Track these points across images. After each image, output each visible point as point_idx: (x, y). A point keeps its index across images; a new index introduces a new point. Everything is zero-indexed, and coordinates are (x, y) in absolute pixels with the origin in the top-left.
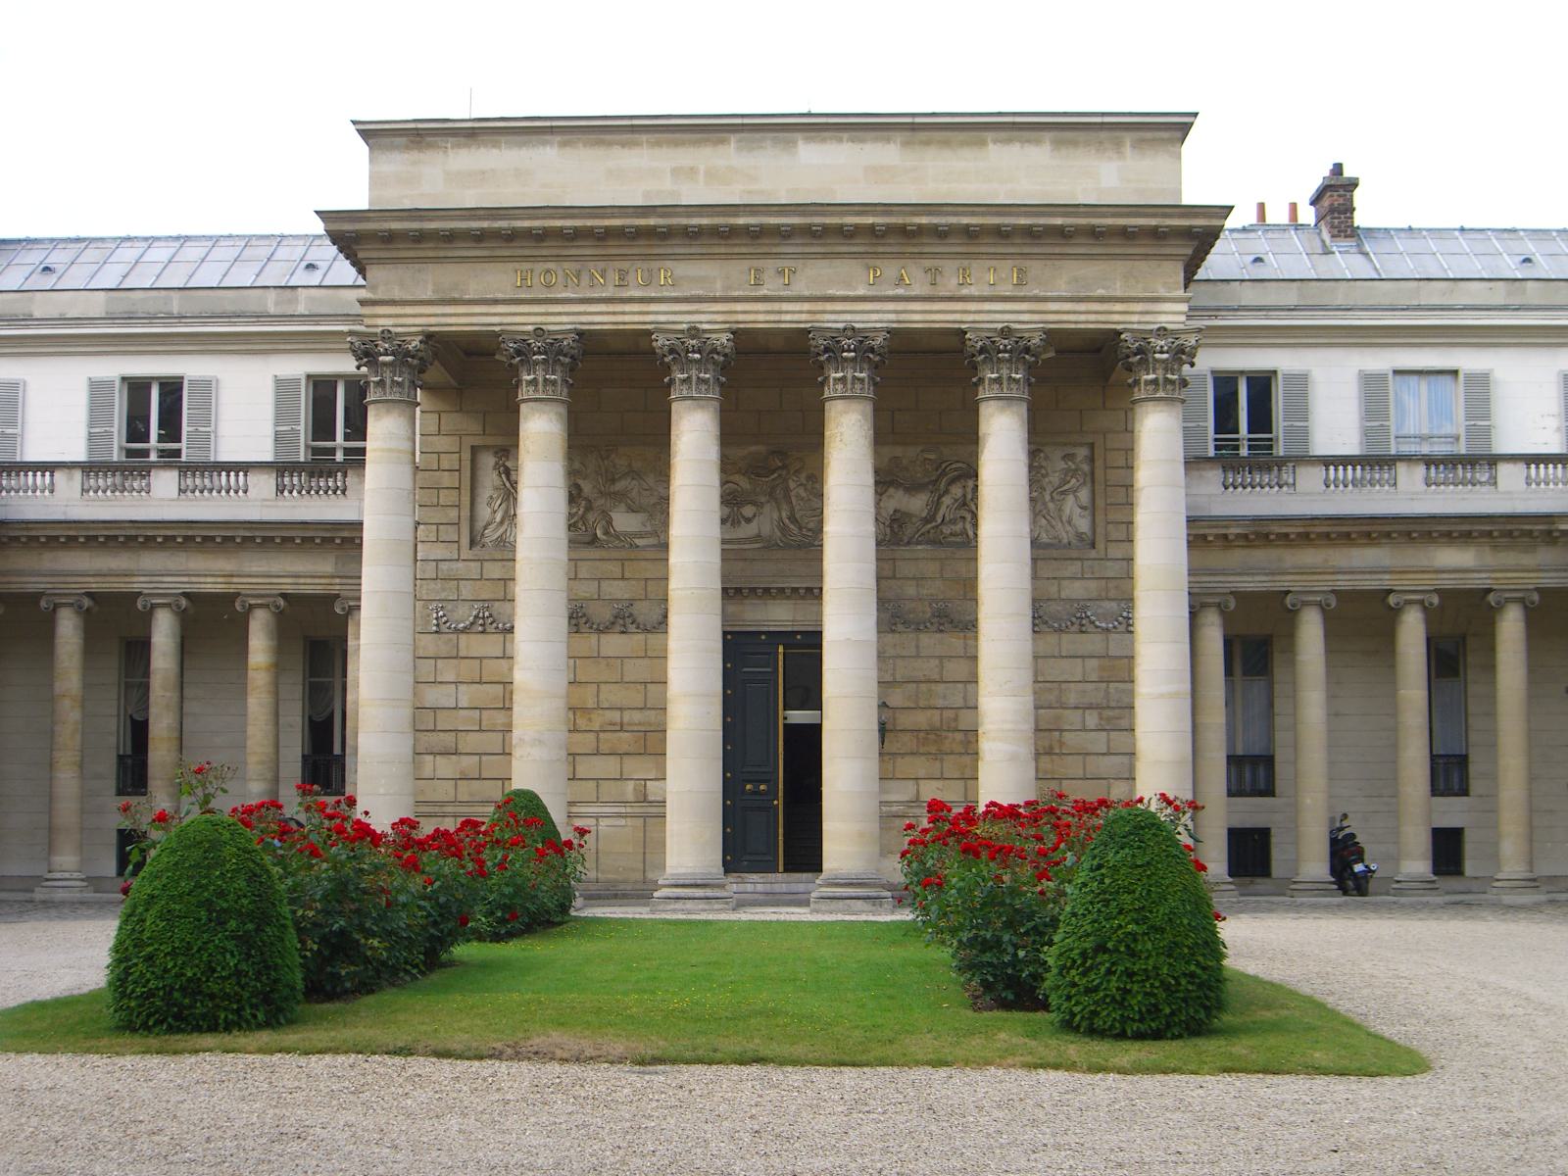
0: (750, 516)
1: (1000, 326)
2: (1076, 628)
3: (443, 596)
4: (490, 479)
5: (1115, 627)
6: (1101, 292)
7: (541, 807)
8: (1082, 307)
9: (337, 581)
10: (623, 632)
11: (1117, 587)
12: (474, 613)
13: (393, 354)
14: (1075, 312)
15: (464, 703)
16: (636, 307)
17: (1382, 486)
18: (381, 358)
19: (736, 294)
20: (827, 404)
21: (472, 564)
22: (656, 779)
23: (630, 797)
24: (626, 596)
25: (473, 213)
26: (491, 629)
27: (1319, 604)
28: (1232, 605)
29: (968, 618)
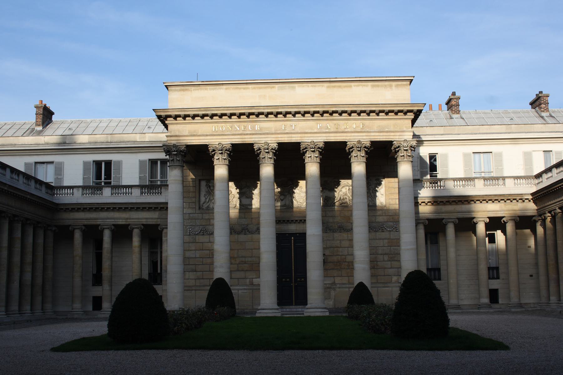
2: (380, 230)
3: (191, 224)
6: (387, 130)
8: (382, 134)
15: (198, 256)
23: (248, 283)
26: (205, 234)
27: (423, 223)
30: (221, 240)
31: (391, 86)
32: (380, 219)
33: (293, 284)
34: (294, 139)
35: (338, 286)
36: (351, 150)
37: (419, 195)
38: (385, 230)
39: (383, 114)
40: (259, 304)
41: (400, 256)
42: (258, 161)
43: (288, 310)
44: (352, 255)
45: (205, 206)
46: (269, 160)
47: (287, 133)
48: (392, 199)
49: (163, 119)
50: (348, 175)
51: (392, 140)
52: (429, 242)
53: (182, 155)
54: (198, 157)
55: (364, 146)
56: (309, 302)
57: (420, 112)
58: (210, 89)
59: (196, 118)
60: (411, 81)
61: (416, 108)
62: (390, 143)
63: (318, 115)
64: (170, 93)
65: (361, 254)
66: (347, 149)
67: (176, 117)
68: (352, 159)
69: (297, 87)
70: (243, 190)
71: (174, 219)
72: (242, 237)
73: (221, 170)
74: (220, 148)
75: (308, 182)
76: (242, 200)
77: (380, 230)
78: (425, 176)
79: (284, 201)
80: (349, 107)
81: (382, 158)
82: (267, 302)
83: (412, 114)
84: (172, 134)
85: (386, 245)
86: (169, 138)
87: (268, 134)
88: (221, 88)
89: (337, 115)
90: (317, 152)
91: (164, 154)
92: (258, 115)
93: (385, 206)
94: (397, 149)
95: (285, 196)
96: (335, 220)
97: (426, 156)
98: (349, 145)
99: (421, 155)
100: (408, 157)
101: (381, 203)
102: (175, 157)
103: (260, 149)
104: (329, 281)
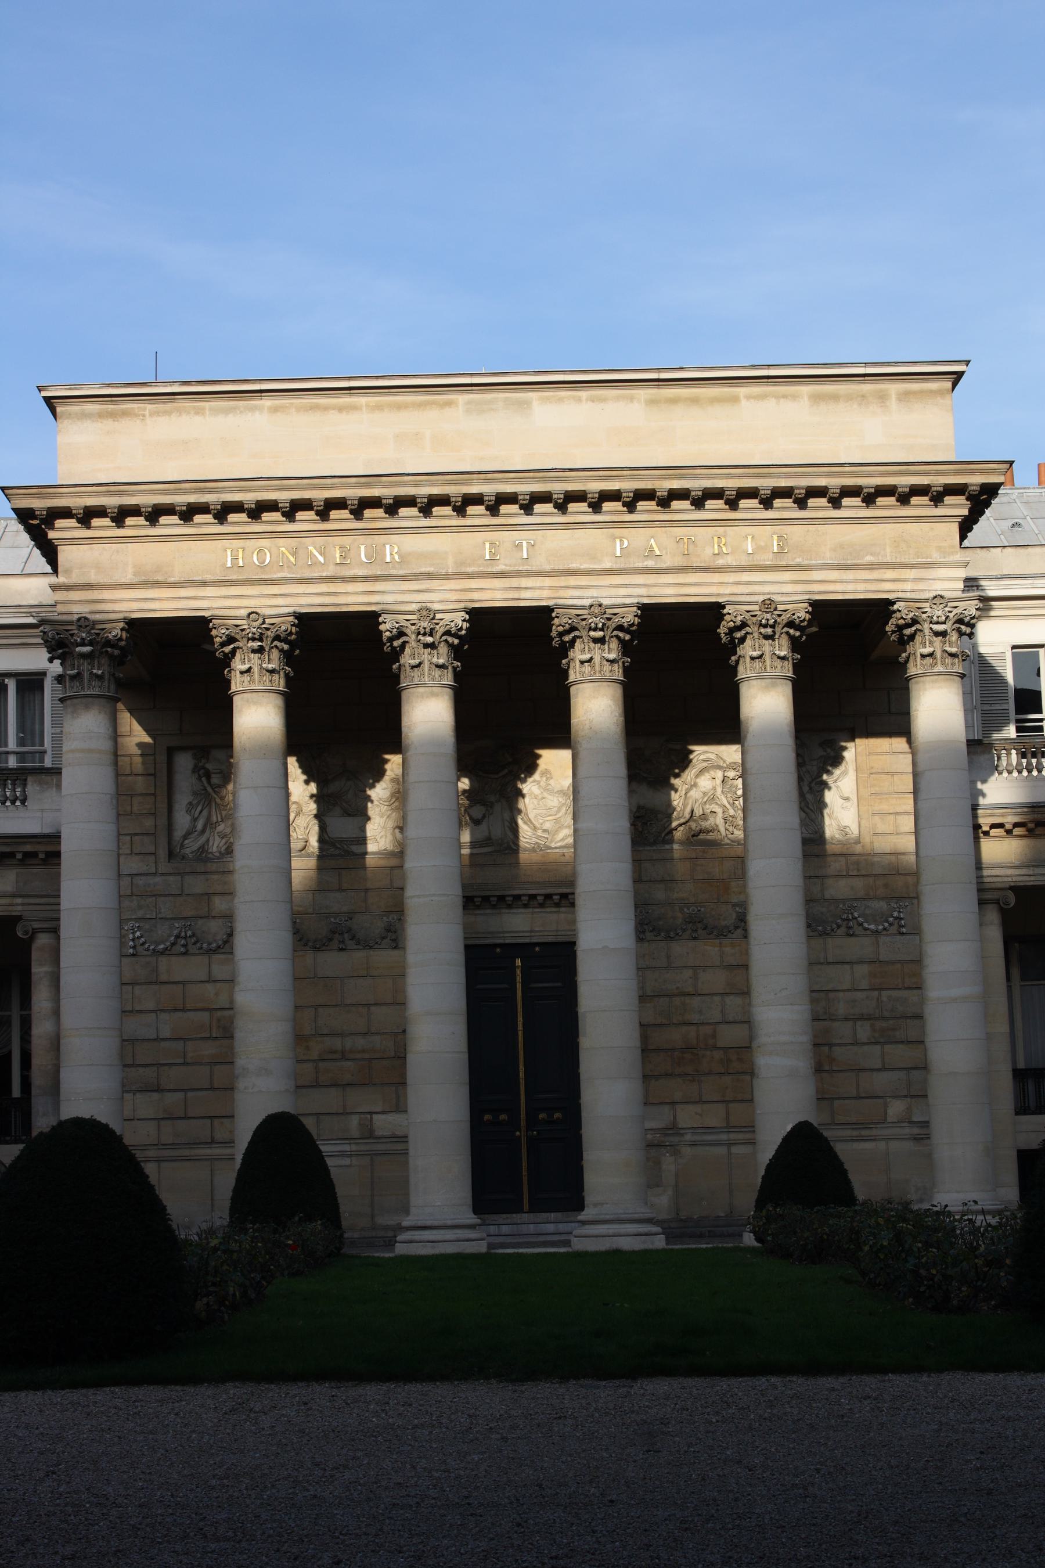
0: (480, 817)
1: (761, 598)
2: (842, 931)
3: (140, 914)
4: (185, 782)
5: (885, 929)
6: (869, 559)
7: (811, 1124)
8: (850, 575)
9: (19, 901)
10: (341, 949)
11: (886, 886)
12: (176, 932)
13: (90, 644)
14: (842, 581)
15: (166, 1032)
16: (361, 587)
17: (1000, 773)
18: (78, 649)
19: (470, 570)
20: (572, 689)
21: (171, 878)
22: (383, 1112)
23: (355, 1133)
24: (345, 909)
25: (178, 486)
26: (192, 949)
27: (997, 902)
28: (1012, 901)
29: (723, 923)
30: (260, 971)
31: (882, 397)
32: (840, 889)
33: (521, 1134)
34: (530, 594)
35: (688, 1137)
36: (738, 635)
37: (981, 801)
38: (858, 930)
39: (857, 501)
40: (407, 1211)
41: (923, 1027)
42: (396, 678)
43: (505, 1229)
44: (748, 1022)
45: (192, 846)
46: (437, 672)
47: (503, 575)
48: (883, 814)
49: (38, 525)
50: (727, 727)
51: (890, 596)
52: (1016, 972)
53: (111, 657)
54: (168, 669)
55: (785, 618)
56: (589, 1198)
57: (990, 491)
58: (215, 412)
59: (163, 520)
60: (957, 377)
61: (976, 480)
62: (883, 608)
63: (617, 506)
64: (64, 424)
65: (778, 1018)
66: (722, 630)
67: (87, 516)
68: (741, 668)
69: (535, 404)
70: (333, 787)
71: (84, 894)
72: (331, 962)
73: (257, 716)
74: (253, 629)
75: (583, 754)
76: (328, 820)
77: (842, 931)
78: (999, 728)
79: (484, 826)
80: (729, 476)
81: (853, 663)
82: (434, 1199)
83: (961, 499)
84: (74, 579)
85: (864, 985)
86: (61, 596)
87: (429, 576)
88: (253, 409)
89: (686, 504)
90: (614, 644)
91: (43, 654)
92: (393, 507)
93: (858, 841)
94: (907, 632)
95: (488, 805)
96: (683, 895)
97: (1002, 654)
98: (733, 614)
99: (982, 650)
100: (949, 660)
101: (843, 830)
102: (85, 666)
103: (401, 634)
104: (660, 1119)
